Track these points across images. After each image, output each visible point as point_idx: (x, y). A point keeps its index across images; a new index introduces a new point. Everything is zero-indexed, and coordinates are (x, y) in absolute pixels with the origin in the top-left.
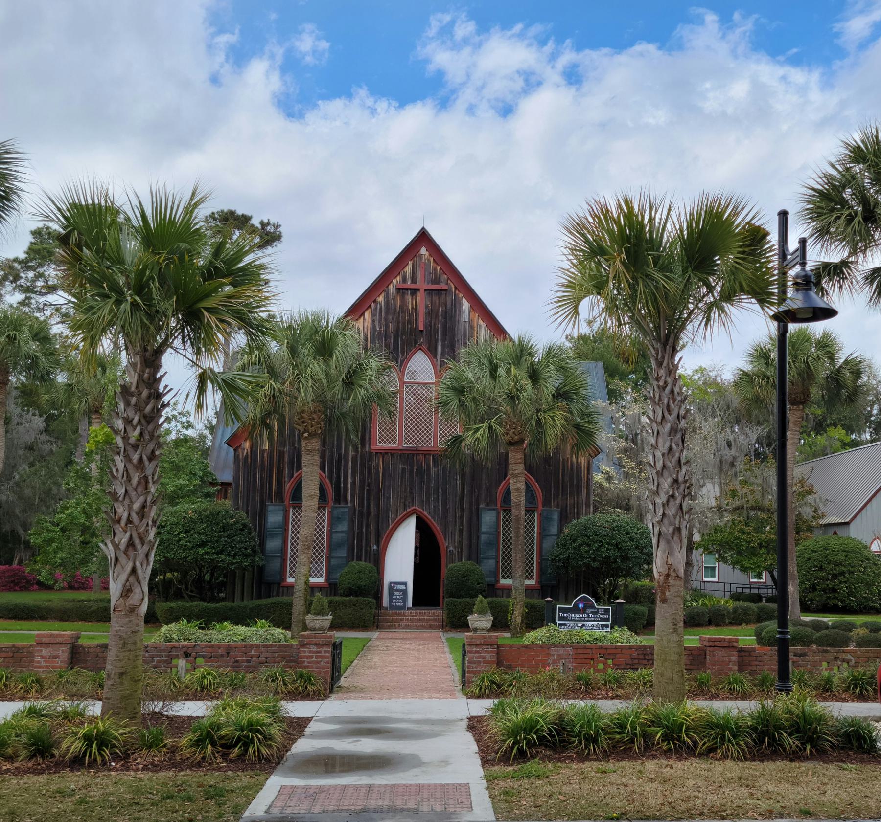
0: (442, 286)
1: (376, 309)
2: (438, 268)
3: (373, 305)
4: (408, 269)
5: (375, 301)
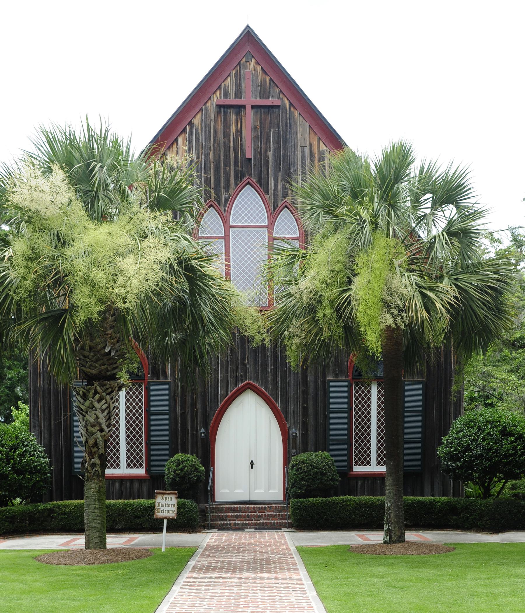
0: (273, 101)
1: (191, 133)
2: (268, 79)
3: (188, 128)
4: (230, 83)
5: (191, 123)
